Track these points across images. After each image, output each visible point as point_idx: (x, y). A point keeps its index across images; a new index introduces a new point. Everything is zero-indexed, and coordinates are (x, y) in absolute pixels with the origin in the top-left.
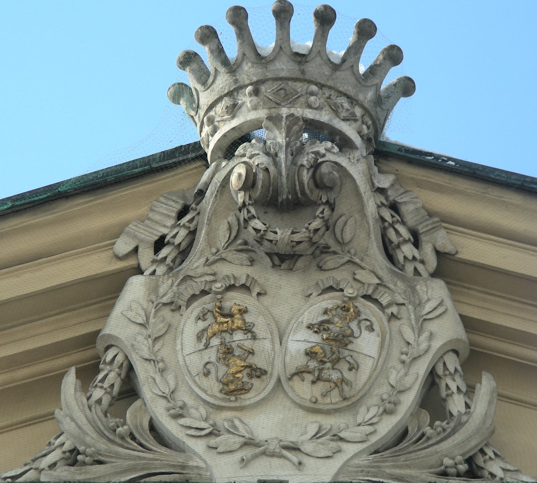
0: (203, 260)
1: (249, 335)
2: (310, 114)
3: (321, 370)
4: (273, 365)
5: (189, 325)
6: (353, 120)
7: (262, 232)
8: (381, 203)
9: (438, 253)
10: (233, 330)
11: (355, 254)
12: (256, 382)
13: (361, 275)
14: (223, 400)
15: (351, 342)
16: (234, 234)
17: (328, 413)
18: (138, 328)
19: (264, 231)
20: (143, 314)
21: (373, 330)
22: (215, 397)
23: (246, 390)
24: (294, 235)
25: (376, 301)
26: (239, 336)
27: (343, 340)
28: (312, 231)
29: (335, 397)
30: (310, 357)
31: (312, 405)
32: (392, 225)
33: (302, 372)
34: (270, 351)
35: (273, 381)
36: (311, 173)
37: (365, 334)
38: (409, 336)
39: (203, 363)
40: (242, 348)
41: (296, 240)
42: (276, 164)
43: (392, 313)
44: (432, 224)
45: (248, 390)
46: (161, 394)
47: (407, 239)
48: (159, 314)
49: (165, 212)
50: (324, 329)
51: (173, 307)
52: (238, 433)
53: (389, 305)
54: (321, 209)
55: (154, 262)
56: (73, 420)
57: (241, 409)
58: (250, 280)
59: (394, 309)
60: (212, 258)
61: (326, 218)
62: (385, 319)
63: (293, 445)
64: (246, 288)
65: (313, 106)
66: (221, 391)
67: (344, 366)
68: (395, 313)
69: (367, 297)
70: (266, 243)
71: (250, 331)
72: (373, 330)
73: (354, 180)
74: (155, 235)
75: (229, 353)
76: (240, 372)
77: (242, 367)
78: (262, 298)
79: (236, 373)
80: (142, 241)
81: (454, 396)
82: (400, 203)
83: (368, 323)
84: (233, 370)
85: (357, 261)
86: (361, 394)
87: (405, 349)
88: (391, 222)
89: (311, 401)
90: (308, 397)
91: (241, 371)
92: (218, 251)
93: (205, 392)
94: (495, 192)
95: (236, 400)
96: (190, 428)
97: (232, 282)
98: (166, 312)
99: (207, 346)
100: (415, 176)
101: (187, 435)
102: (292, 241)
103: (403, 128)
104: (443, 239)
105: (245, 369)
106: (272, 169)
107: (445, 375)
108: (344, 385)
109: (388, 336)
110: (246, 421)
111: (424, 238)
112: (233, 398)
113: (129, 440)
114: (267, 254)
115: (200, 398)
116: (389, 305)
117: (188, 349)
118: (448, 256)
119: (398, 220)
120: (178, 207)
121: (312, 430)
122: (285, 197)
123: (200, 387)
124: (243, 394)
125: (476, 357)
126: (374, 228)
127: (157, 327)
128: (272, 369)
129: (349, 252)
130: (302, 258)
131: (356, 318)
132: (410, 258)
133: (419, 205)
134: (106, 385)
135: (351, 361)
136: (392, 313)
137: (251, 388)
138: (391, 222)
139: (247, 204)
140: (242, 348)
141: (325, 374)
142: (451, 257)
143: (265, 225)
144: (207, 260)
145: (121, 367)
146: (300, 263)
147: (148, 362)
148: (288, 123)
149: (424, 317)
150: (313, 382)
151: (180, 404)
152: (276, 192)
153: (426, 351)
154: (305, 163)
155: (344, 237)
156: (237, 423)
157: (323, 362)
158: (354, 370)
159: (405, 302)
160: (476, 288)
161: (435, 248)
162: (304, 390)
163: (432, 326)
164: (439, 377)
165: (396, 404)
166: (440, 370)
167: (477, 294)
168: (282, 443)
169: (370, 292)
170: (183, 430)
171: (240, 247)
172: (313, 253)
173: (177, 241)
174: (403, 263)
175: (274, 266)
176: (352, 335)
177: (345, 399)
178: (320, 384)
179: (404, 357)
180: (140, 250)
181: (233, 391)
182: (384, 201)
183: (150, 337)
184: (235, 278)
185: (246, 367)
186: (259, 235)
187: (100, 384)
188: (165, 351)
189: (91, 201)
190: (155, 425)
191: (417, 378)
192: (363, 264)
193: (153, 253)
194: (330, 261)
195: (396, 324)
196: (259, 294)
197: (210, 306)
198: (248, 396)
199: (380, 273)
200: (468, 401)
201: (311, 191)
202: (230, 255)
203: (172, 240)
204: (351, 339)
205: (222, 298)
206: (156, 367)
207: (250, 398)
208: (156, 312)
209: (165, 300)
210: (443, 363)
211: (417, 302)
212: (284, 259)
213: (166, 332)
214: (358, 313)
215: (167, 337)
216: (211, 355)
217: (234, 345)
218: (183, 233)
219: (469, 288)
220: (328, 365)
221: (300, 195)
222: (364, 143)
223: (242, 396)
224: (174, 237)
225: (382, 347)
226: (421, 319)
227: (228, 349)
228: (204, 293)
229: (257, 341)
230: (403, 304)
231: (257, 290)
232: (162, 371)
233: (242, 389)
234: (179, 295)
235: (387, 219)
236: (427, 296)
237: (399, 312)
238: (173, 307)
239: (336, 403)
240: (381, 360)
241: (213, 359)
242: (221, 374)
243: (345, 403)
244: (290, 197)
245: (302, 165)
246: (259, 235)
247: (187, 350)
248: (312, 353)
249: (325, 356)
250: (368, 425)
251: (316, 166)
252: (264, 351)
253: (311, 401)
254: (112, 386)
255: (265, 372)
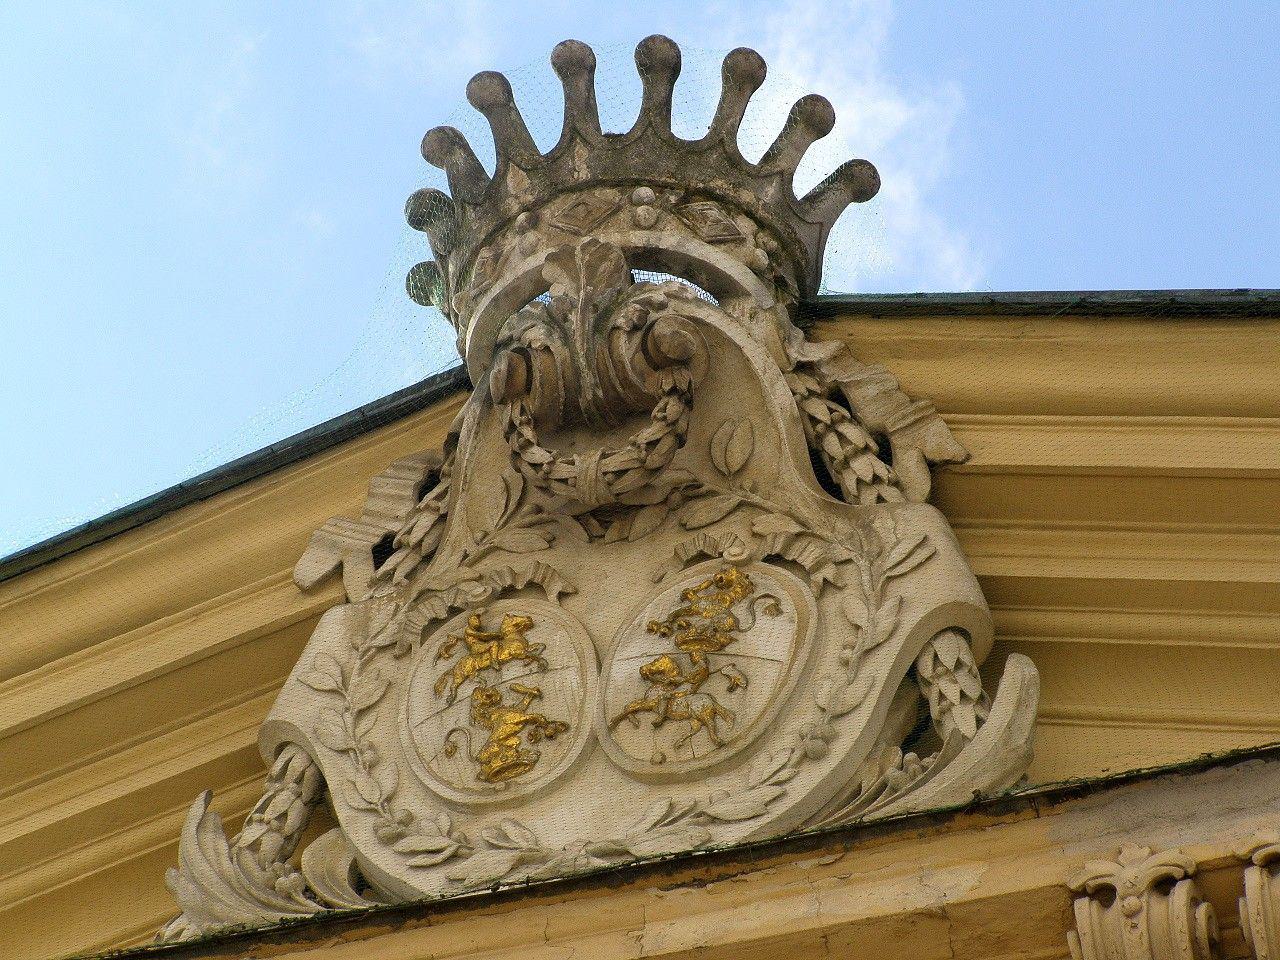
0: (457, 558)
1: (534, 666)
2: (638, 239)
3: (669, 700)
4: (581, 712)
5: (423, 672)
6: (732, 241)
7: (545, 467)
8: (809, 390)
9: (933, 467)
10: (502, 663)
11: (754, 490)
12: (545, 747)
13: (765, 523)
14: (481, 793)
15: (732, 640)
16: (516, 496)
17: (691, 778)
18: (326, 700)
19: (548, 463)
20: (336, 671)
21: (779, 612)
22: (465, 790)
23: (526, 765)
24: (608, 460)
25: (794, 565)
26: (513, 672)
27: (717, 639)
28: (643, 446)
29: (702, 744)
30: (653, 681)
31: (657, 769)
32: (831, 427)
33: (635, 712)
34: (575, 685)
35: (581, 742)
36: (637, 338)
37: (764, 622)
38: (859, 612)
39: (446, 732)
40: (518, 692)
41: (611, 469)
42: (566, 339)
43: (825, 580)
44: (915, 412)
45: (532, 765)
46: (364, 805)
47: (862, 446)
48: (371, 667)
49: (393, 492)
50: (680, 627)
51: (397, 651)
52: (507, 845)
53: (819, 565)
54: (661, 404)
55: (374, 583)
56: (194, 880)
57: (521, 802)
58: (542, 571)
59: (828, 572)
60: (473, 551)
61: (670, 418)
62: (808, 594)
63: (615, 847)
64: (534, 587)
65: (643, 223)
66: (478, 778)
67: (717, 686)
68: (830, 578)
69: (775, 559)
70: (555, 485)
71: (536, 659)
72: (779, 612)
73: (739, 349)
74: (375, 535)
75: (493, 704)
76: (515, 734)
77: (517, 724)
78: (570, 602)
79: (506, 738)
80: (347, 550)
81: (954, 710)
82: (847, 385)
83: (772, 601)
84: (501, 732)
85: (756, 499)
86: (755, 733)
87: (851, 639)
88: (829, 422)
89: (652, 762)
90: (647, 756)
91: (516, 733)
92: (486, 534)
93: (449, 784)
94: (1039, 331)
95: (508, 787)
96: (414, 853)
97: (508, 582)
98: (385, 664)
99: (451, 702)
100: (884, 338)
101: (412, 867)
102: (605, 474)
103: (856, 258)
104: (938, 439)
105: (524, 726)
106: (556, 346)
107: (939, 676)
108: (720, 722)
109: (813, 622)
110: (527, 823)
111: (897, 441)
112: (500, 785)
113: (301, 899)
114: (577, 518)
115: (436, 796)
116: (819, 565)
117: (418, 715)
118: (951, 467)
119: (844, 417)
120: (418, 477)
121: (659, 810)
122: (590, 397)
123: (440, 780)
124: (520, 774)
125: (1002, 629)
126: (789, 434)
127: (364, 689)
128: (580, 718)
129: (741, 487)
130: (644, 511)
131: (744, 597)
132: (868, 478)
133: (891, 385)
134: (268, 815)
135: (733, 673)
136: (825, 580)
137: (536, 762)
138: (829, 422)
139: (517, 423)
140: (518, 692)
141: (679, 705)
142: (957, 469)
143: (550, 452)
144: (466, 556)
145: (299, 781)
146: (641, 523)
147: (345, 757)
148: (587, 257)
149: (889, 574)
150: (657, 726)
151: (399, 816)
152: (574, 388)
153: (891, 634)
154: (621, 321)
155: (729, 460)
156: (510, 829)
157: (676, 685)
158: (739, 690)
159: (852, 555)
160: (1024, 522)
161: (926, 459)
162: (640, 743)
163: (905, 588)
164: (928, 684)
165: (828, 740)
166: (926, 669)
167: (1021, 532)
168: (590, 848)
169: (777, 549)
170: (401, 859)
171: (528, 520)
172: (667, 499)
173: (413, 539)
174: (856, 494)
175: (591, 539)
176: (736, 626)
177: (721, 745)
178: (671, 728)
179: (848, 653)
180: (347, 569)
181: (498, 773)
182: (815, 387)
183: (347, 709)
184: (514, 574)
185: (526, 723)
186: (541, 473)
187: (257, 816)
188: (376, 730)
189: (246, 498)
190: (366, 874)
191: (872, 686)
192: (768, 504)
193: (372, 567)
194: (700, 512)
195: (832, 601)
196: (562, 596)
197: (459, 633)
198: (532, 775)
199: (805, 513)
200: (982, 715)
201: (641, 375)
202: (509, 538)
203: (405, 539)
204: (733, 634)
205: (486, 612)
206: (357, 761)
207: (535, 779)
208: (364, 666)
209: (381, 641)
210: (931, 656)
211: (876, 550)
212: (606, 517)
213: (383, 697)
214: (750, 587)
215: (384, 707)
216: (460, 715)
217: (502, 689)
218: (425, 521)
219: (1008, 527)
220: (687, 687)
221: (620, 389)
222: (768, 287)
223: (518, 780)
224: (409, 532)
225: (798, 642)
226: (883, 578)
227: (489, 697)
228: (454, 611)
229: (549, 675)
230: (849, 561)
231: (557, 587)
232: (371, 767)
233: (516, 765)
234: (404, 628)
235: (819, 416)
236: (896, 535)
237: (838, 575)
238: (397, 651)
239: (704, 757)
240: (798, 666)
241: (464, 722)
242: (477, 746)
243: (723, 754)
244: (600, 393)
245: (616, 328)
246: (541, 473)
247: (417, 718)
248: (653, 673)
249: (680, 674)
250: (773, 785)
251: (641, 327)
252: (567, 691)
253: (652, 762)
254: (283, 816)
255: (566, 727)
